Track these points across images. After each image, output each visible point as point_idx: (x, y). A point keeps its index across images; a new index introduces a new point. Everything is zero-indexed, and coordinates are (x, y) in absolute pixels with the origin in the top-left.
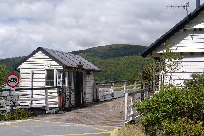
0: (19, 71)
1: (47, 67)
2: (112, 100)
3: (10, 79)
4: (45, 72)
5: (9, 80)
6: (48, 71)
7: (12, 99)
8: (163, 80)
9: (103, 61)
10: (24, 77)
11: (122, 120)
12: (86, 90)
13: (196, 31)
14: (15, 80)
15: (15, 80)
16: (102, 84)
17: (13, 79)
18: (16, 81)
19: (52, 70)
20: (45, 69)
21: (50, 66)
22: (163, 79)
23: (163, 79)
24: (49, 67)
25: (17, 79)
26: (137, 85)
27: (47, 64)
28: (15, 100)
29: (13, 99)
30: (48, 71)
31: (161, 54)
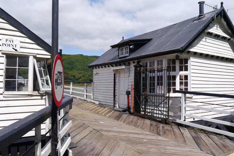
1: (10, 50)
4: (3, 60)
6: (11, 58)
10: (97, 79)
11: (123, 130)
13: (124, 109)
19: (24, 60)
20: (3, 54)
21: (18, 48)
23: (83, 93)
26: (148, 89)
27: (8, 43)
30: (11, 58)
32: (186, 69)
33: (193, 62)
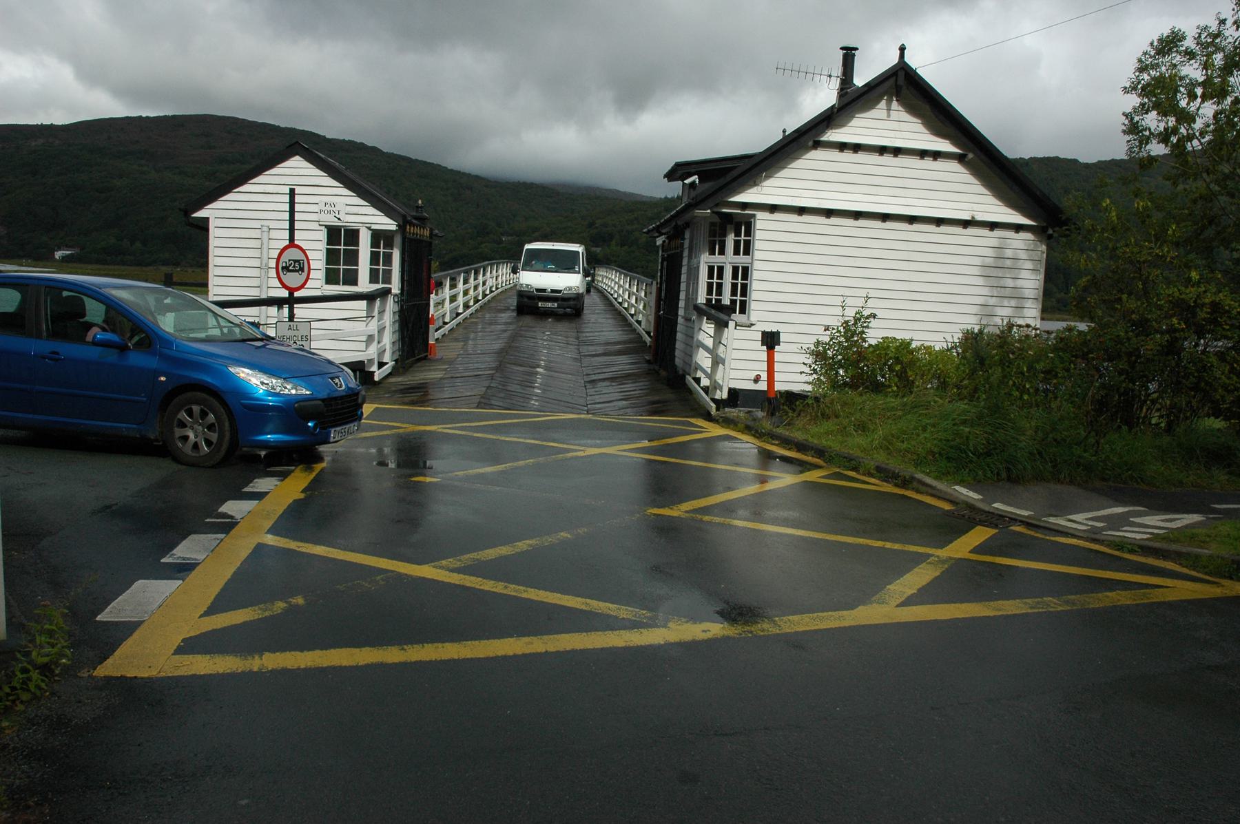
0: (207, 230)
2: (528, 389)
3: (286, 263)
5: (284, 265)
7: (291, 333)
8: (739, 298)
9: (1232, 303)
12: (585, 301)
14: (300, 264)
15: (300, 264)
16: (659, 274)
17: (295, 261)
18: (302, 269)
19: (353, 235)
22: (739, 295)
24: (339, 219)
25: (306, 261)
28: (300, 339)
29: (295, 333)
31: (745, 206)
32: (747, 252)
33: (763, 223)
